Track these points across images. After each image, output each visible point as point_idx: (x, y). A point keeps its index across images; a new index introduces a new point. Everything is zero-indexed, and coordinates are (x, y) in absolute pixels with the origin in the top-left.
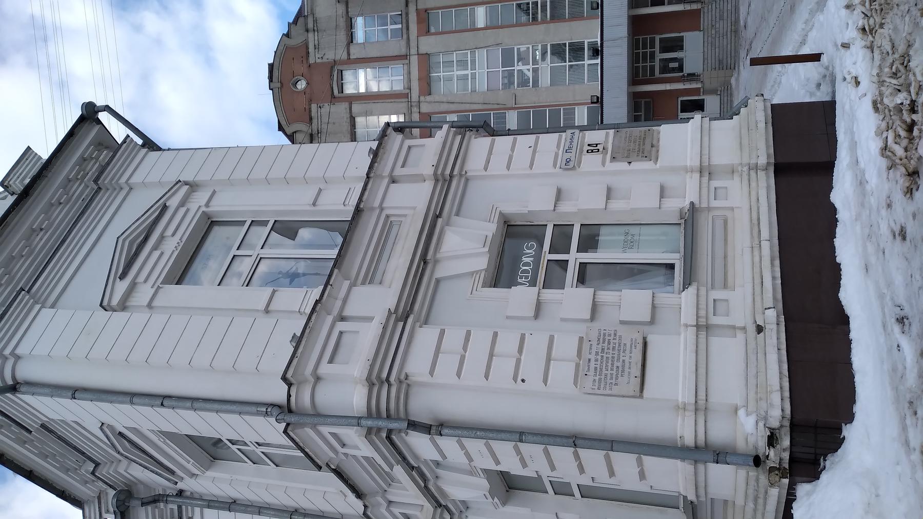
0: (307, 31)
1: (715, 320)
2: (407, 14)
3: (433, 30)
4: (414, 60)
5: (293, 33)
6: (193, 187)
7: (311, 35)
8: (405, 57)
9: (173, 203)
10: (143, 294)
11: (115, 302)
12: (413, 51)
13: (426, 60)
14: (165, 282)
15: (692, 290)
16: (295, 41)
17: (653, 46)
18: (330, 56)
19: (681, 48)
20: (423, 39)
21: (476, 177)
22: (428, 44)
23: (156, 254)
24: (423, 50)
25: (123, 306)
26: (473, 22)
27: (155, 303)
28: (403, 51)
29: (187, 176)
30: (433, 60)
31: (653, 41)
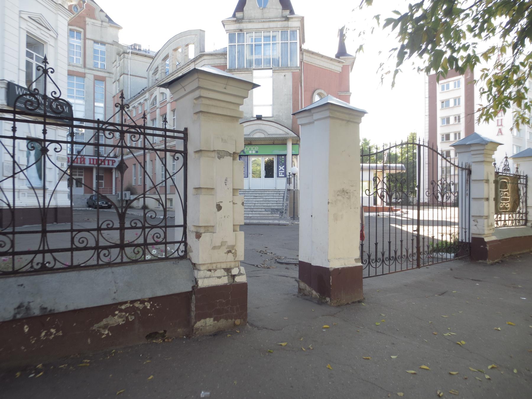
0: (102, 21)
1: (21, 193)
2: (105, 72)
3: (96, 81)
4: (82, 70)
5: (101, 13)
6: (56, 39)
7: (100, 22)
8: (85, 66)
9: (51, 33)
10: (24, 25)
11: (22, 16)
12: (87, 71)
13: (83, 76)
14: (27, 32)
15: (28, 188)
16: (97, 13)
17: (79, 175)
18: (88, 28)
19: (77, 186)
20: (92, 77)
21: (56, 132)
22: (90, 78)
23: (35, 28)
24: (87, 75)
25: (20, 17)
26: (97, 102)
27: (21, 30)
28: (87, 66)
29: (59, 38)
30: (82, 79)
31: (82, 175)
